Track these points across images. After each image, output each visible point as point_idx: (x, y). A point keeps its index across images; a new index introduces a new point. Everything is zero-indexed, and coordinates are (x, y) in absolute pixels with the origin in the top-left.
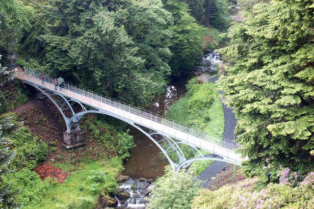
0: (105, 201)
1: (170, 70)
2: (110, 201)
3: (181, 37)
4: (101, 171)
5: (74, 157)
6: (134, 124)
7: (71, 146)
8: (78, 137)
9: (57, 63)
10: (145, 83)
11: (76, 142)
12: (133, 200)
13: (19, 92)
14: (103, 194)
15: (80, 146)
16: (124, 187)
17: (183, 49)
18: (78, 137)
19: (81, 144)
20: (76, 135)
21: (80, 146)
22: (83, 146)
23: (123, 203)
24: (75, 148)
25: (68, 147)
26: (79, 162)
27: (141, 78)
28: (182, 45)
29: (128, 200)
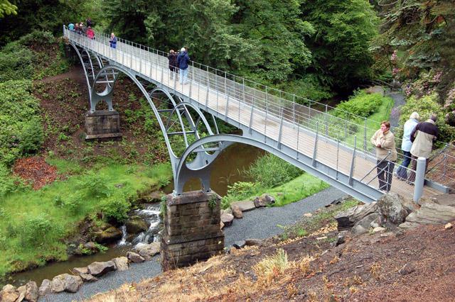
0: (94, 231)
1: (310, 56)
2: (101, 232)
3: (349, 28)
4: (128, 179)
5: (90, 154)
6: (137, 77)
7: (93, 137)
8: (109, 123)
9: (253, 87)
10: (229, 42)
11: (105, 131)
12: (148, 236)
13: (58, 57)
14: (93, 216)
15: (110, 139)
16: (150, 211)
17: (352, 46)
18: (109, 123)
19: (113, 135)
20: (103, 118)
21: (110, 139)
22: (116, 139)
23: (129, 240)
24: (100, 140)
25: (87, 137)
26: (95, 161)
27: (226, 35)
28: (351, 41)
29: (141, 236)
